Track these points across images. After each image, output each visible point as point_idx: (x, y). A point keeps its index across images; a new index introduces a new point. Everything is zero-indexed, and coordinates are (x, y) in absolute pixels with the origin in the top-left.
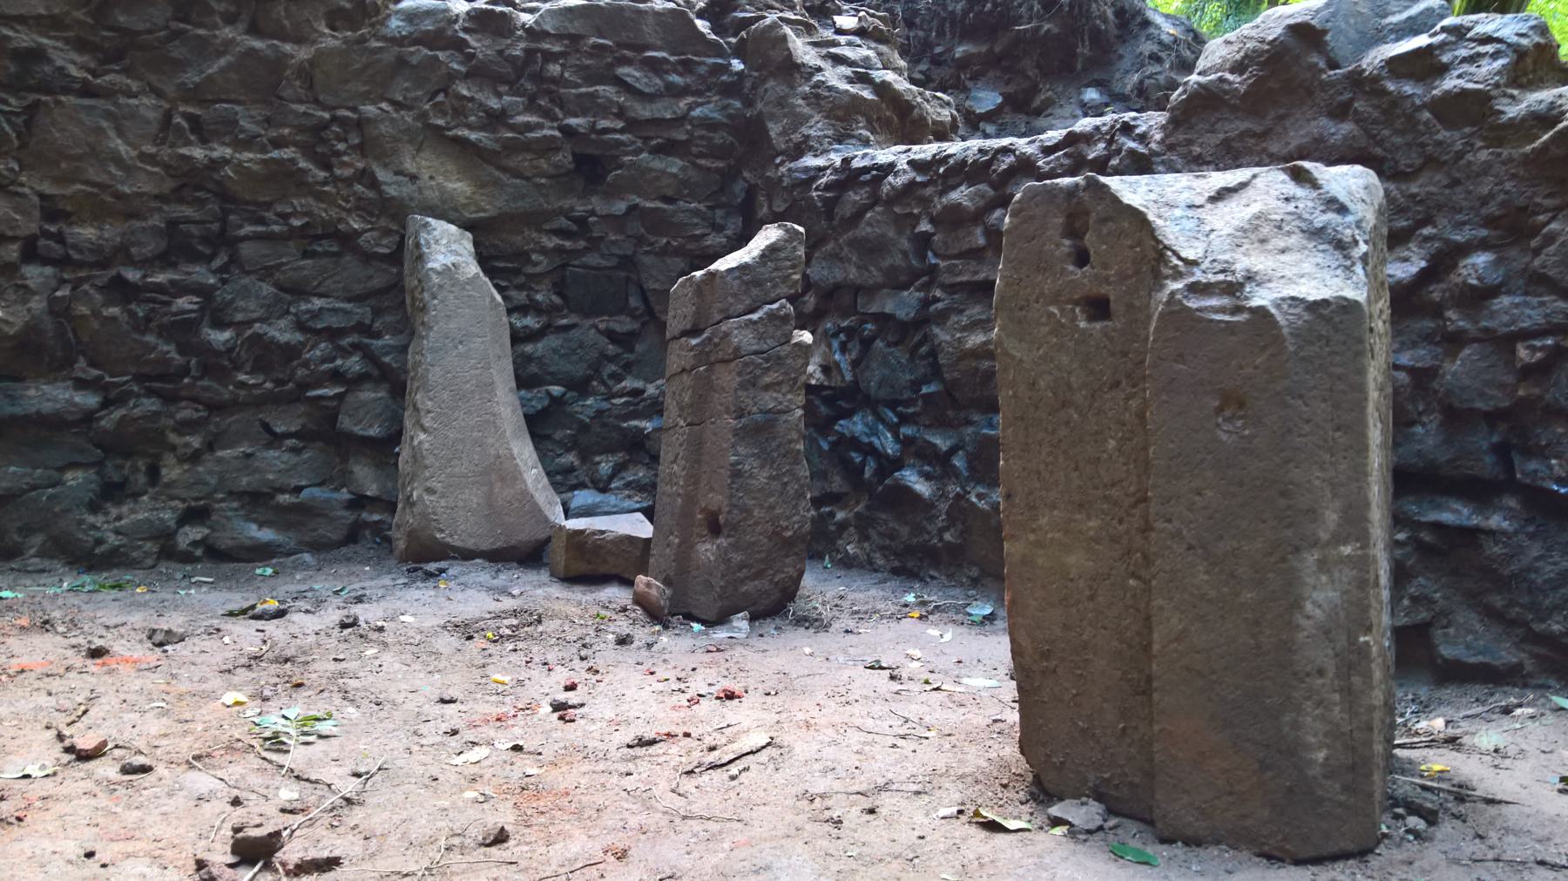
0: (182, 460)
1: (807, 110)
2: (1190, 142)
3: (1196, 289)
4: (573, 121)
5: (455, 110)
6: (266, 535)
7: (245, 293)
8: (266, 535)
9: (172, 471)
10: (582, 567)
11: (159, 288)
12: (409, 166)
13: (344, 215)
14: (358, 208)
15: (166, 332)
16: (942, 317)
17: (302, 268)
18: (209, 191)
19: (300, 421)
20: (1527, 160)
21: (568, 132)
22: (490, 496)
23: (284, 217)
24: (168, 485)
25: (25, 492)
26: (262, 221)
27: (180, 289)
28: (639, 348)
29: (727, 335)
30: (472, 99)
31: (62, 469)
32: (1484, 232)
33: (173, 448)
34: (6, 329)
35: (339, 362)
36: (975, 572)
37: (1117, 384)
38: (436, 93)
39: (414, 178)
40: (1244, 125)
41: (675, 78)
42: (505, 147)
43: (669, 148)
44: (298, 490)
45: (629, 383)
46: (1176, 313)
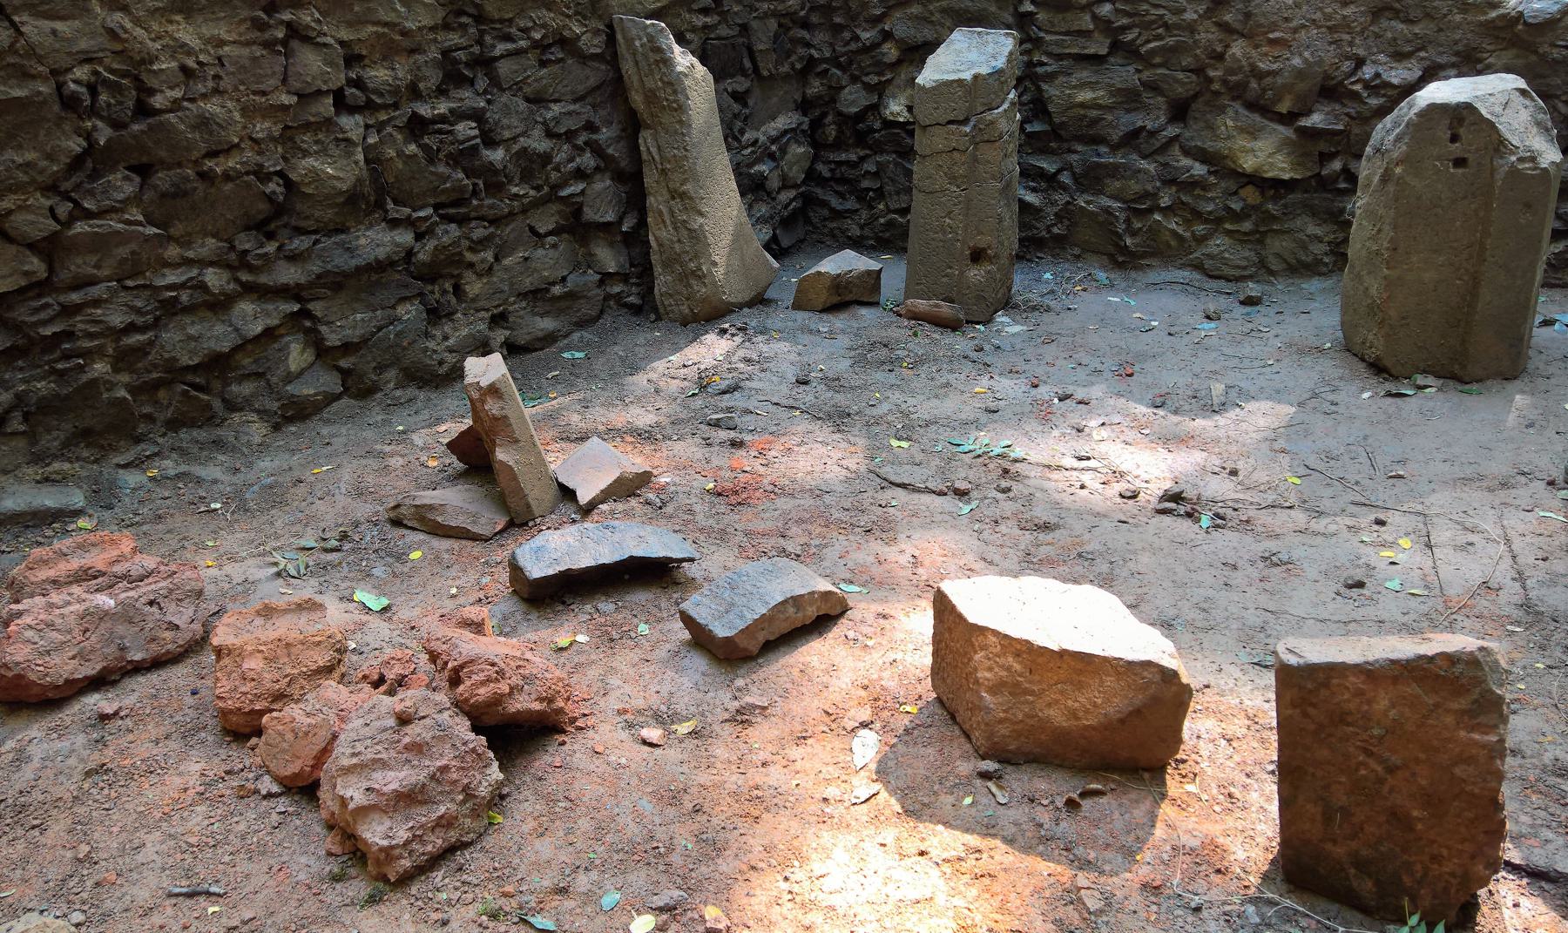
0: (480, 276)
3: (1521, 160)
6: (547, 324)
7: (507, 110)
8: (547, 324)
9: (474, 287)
10: (836, 299)
11: (442, 119)
14: (577, 13)
15: (455, 160)
16: (1050, 77)
18: (470, 15)
19: (554, 219)
20: (1481, 24)
22: (742, 259)
23: (525, 30)
24: (473, 300)
25: (373, 334)
26: (508, 38)
27: (458, 115)
28: (751, 102)
29: (992, 123)
31: (393, 307)
32: (1454, 59)
33: (471, 265)
34: (338, 185)
36: (1077, 251)
37: (1465, 197)
44: (564, 279)
45: (748, 136)
46: (1514, 172)
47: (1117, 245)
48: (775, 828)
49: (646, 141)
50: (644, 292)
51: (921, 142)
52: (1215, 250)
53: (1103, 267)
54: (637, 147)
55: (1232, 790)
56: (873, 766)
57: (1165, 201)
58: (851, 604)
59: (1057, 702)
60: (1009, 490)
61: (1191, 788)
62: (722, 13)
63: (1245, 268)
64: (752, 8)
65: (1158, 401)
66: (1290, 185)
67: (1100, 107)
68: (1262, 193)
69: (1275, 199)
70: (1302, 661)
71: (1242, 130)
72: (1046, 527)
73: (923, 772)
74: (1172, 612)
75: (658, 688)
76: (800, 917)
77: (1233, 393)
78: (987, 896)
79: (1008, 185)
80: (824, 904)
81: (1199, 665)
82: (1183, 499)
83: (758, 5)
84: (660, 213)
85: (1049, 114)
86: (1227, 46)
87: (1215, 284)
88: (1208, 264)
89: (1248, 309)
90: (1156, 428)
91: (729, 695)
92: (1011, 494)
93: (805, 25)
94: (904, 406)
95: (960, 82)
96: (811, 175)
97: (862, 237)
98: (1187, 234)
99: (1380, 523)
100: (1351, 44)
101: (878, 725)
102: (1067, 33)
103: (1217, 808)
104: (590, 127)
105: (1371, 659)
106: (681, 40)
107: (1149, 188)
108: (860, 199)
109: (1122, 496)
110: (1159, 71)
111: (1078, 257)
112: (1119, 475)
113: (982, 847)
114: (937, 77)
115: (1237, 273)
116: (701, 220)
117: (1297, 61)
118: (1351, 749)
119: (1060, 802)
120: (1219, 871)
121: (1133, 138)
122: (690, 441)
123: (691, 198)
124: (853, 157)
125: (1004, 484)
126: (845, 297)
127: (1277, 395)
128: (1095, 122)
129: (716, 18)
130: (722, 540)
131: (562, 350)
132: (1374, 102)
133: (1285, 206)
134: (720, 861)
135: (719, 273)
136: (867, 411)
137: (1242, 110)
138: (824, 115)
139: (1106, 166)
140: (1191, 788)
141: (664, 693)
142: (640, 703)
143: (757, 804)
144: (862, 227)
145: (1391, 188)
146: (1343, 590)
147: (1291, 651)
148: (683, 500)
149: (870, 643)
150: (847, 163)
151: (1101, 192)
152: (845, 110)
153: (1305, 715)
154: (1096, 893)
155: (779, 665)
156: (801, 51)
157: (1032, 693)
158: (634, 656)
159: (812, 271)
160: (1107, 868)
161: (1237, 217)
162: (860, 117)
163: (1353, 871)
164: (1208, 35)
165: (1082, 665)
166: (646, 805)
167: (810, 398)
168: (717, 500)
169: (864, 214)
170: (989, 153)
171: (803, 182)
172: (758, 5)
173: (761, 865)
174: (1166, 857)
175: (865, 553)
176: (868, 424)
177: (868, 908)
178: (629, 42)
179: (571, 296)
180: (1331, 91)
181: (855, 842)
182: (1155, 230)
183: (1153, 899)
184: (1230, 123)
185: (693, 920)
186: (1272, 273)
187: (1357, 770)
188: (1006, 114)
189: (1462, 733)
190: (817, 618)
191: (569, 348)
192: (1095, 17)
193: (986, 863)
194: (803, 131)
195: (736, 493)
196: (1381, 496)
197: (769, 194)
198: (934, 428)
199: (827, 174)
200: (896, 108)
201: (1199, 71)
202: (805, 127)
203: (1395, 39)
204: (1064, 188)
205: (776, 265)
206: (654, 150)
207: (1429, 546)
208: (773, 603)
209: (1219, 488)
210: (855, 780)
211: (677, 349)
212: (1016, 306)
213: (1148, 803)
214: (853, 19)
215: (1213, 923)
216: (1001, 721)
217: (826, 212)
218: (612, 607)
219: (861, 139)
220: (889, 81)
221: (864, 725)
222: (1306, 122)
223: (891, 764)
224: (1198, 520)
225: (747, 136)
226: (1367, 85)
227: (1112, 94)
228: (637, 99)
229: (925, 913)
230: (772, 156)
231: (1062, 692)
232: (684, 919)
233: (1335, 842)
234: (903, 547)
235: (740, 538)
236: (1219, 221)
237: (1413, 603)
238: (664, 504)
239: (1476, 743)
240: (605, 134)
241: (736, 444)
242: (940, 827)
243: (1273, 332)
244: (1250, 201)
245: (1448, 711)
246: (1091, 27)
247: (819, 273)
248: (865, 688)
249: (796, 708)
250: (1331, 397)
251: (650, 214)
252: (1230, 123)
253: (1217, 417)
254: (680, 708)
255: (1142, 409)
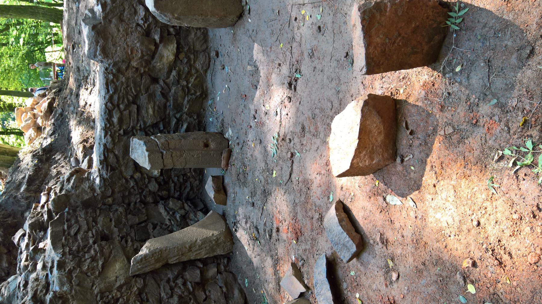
1: (80, 189)
2: (112, 53)
4: (91, 241)
5: (92, 270)
6: (236, 292)
8: (236, 292)
10: (222, 191)
12: (114, 278)
13: (133, 293)
14: (130, 289)
16: (145, 123)
17: (153, 301)
21: (94, 243)
28: (156, 222)
29: (162, 144)
30: (88, 266)
35: (180, 285)
36: (202, 110)
38: (88, 276)
39: (117, 277)
40: (110, 41)
41: (73, 222)
42: (103, 256)
43: (95, 221)
44: (221, 287)
45: (167, 223)
47: (200, 98)
48: (428, 236)
49: (172, 261)
50: (223, 257)
51: (169, 167)
52: (200, 66)
53: (207, 101)
54: (174, 264)
55: (401, 77)
56: (401, 198)
57: (185, 83)
58: (338, 199)
59: (375, 139)
60: (290, 139)
61: (401, 91)
62: (127, 236)
63: (206, 56)
64: (125, 224)
65: (255, 87)
66: (178, 44)
67: (154, 106)
68: (181, 52)
69: (183, 48)
70: (365, 67)
71: (161, 61)
72: (303, 128)
73: (402, 182)
74: (333, 90)
75: (376, 272)
76: (464, 233)
77: (251, 63)
78: (450, 166)
79: (183, 137)
80: (458, 224)
81: (354, 84)
82: (290, 82)
83: (123, 222)
84: (196, 254)
85: (156, 123)
86: (133, 67)
87: (211, 65)
88: (205, 68)
89: (220, 55)
90: (265, 88)
91: (377, 246)
92: (292, 139)
93: (129, 204)
94: (260, 171)
95: (149, 156)
96: (179, 198)
97: (199, 180)
98: (195, 75)
99: (296, 19)
100: (132, 28)
101: (384, 195)
102: (130, 119)
103: (409, 83)
104: (168, 281)
105: (363, 45)
106: (137, 251)
107: (180, 89)
108: (186, 182)
109: (290, 102)
110: (142, 88)
111: (204, 110)
112: (282, 102)
113: (430, 165)
114: (147, 163)
115: (207, 58)
116: (198, 241)
117: (138, 45)
118: (393, 48)
119: (411, 137)
120: (433, 85)
121: (164, 95)
122: (277, 246)
123: (191, 245)
124: (173, 185)
125: (288, 141)
126: (221, 188)
127: (251, 49)
128: (159, 107)
129: (129, 237)
130: (315, 240)
131: (245, 287)
132: (151, 19)
133: (185, 45)
134: (444, 259)
135: (216, 233)
136: (263, 183)
137: (154, 61)
138: (159, 196)
139: (174, 103)
140: (401, 91)
141: (378, 269)
142: (382, 279)
143: (418, 242)
144: (196, 180)
145: (182, 17)
146: (321, 33)
147: (361, 70)
148: (300, 252)
149: (352, 194)
150: (174, 187)
151: (182, 104)
152: (157, 189)
153: (383, 64)
154: (446, 128)
155: (364, 227)
156: (138, 205)
157: (373, 147)
158: (363, 278)
159: (213, 200)
160: (435, 123)
161: (189, 60)
162: (159, 184)
163: (432, 43)
164: (130, 73)
165: (364, 132)
166: (423, 282)
167: (259, 203)
168: (300, 240)
169: (191, 180)
170: (172, 144)
171: (181, 201)
172: (123, 222)
173: (444, 244)
174: (429, 103)
175: (316, 191)
176: (268, 184)
177: (459, 209)
178: (139, 270)
179: (226, 284)
180: (147, 33)
181: (432, 209)
182: (194, 86)
183: (446, 108)
184: (159, 64)
185: (468, 271)
186: (207, 48)
187: (400, 45)
188: (159, 139)
189: (387, 14)
190: (344, 211)
191: (244, 284)
192: (125, 110)
193: (437, 164)
194: (165, 202)
195: (297, 233)
196: (286, 17)
197: (186, 214)
198: (268, 162)
199: (178, 193)
200: (156, 173)
201: (142, 75)
202: (163, 202)
203: (130, 14)
204: (181, 116)
205: (211, 212)
206: (175, 259)
207: (304, 4)
208: (342, 230)
209: (285, 70)
210: (407, 205)
211: (243, 247)
212: (222, 131)
213: (409, 107)
214: (126, 188)
215: (454, 89)
216: (383, 156)
217: (191, 193)
218: (344, 284)
219: (166, 183)
220: (147, 175)
221: (385, 199)
222: (158, 40)
223: (399, 192)
224: (298, 78)
225: (167, 223)
226: (145, 22)
227: (150, 102)
228: (158, 265)
229: (459, 189)
230: (174, 213)
231: (372, 137)
232: (468, 273)
233: (423, 50)
234: (314, 177)
235: (314, 233)
236: (190, 65)
237: (326, 12)
238: (302, 259)
239: (390, 9)
240: (170, 276)
241: (278, 230)
242: (424, 179)
243: (228, 48)
244: (184, 56)
245: (380, 19)
246: (128, 111)
247: (214, 198)
248: (370, 197)
249: (379, 223)
250: (251, 32)
251: (197, 258)
252: (159, 64)
253: (260, 69)
254: (383, 264)
255: (258, 93)
